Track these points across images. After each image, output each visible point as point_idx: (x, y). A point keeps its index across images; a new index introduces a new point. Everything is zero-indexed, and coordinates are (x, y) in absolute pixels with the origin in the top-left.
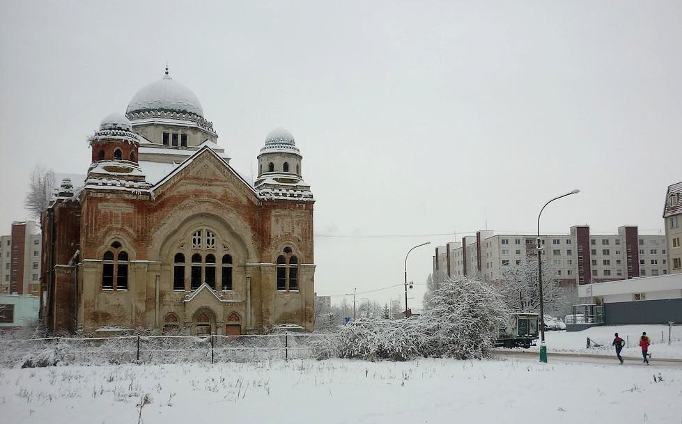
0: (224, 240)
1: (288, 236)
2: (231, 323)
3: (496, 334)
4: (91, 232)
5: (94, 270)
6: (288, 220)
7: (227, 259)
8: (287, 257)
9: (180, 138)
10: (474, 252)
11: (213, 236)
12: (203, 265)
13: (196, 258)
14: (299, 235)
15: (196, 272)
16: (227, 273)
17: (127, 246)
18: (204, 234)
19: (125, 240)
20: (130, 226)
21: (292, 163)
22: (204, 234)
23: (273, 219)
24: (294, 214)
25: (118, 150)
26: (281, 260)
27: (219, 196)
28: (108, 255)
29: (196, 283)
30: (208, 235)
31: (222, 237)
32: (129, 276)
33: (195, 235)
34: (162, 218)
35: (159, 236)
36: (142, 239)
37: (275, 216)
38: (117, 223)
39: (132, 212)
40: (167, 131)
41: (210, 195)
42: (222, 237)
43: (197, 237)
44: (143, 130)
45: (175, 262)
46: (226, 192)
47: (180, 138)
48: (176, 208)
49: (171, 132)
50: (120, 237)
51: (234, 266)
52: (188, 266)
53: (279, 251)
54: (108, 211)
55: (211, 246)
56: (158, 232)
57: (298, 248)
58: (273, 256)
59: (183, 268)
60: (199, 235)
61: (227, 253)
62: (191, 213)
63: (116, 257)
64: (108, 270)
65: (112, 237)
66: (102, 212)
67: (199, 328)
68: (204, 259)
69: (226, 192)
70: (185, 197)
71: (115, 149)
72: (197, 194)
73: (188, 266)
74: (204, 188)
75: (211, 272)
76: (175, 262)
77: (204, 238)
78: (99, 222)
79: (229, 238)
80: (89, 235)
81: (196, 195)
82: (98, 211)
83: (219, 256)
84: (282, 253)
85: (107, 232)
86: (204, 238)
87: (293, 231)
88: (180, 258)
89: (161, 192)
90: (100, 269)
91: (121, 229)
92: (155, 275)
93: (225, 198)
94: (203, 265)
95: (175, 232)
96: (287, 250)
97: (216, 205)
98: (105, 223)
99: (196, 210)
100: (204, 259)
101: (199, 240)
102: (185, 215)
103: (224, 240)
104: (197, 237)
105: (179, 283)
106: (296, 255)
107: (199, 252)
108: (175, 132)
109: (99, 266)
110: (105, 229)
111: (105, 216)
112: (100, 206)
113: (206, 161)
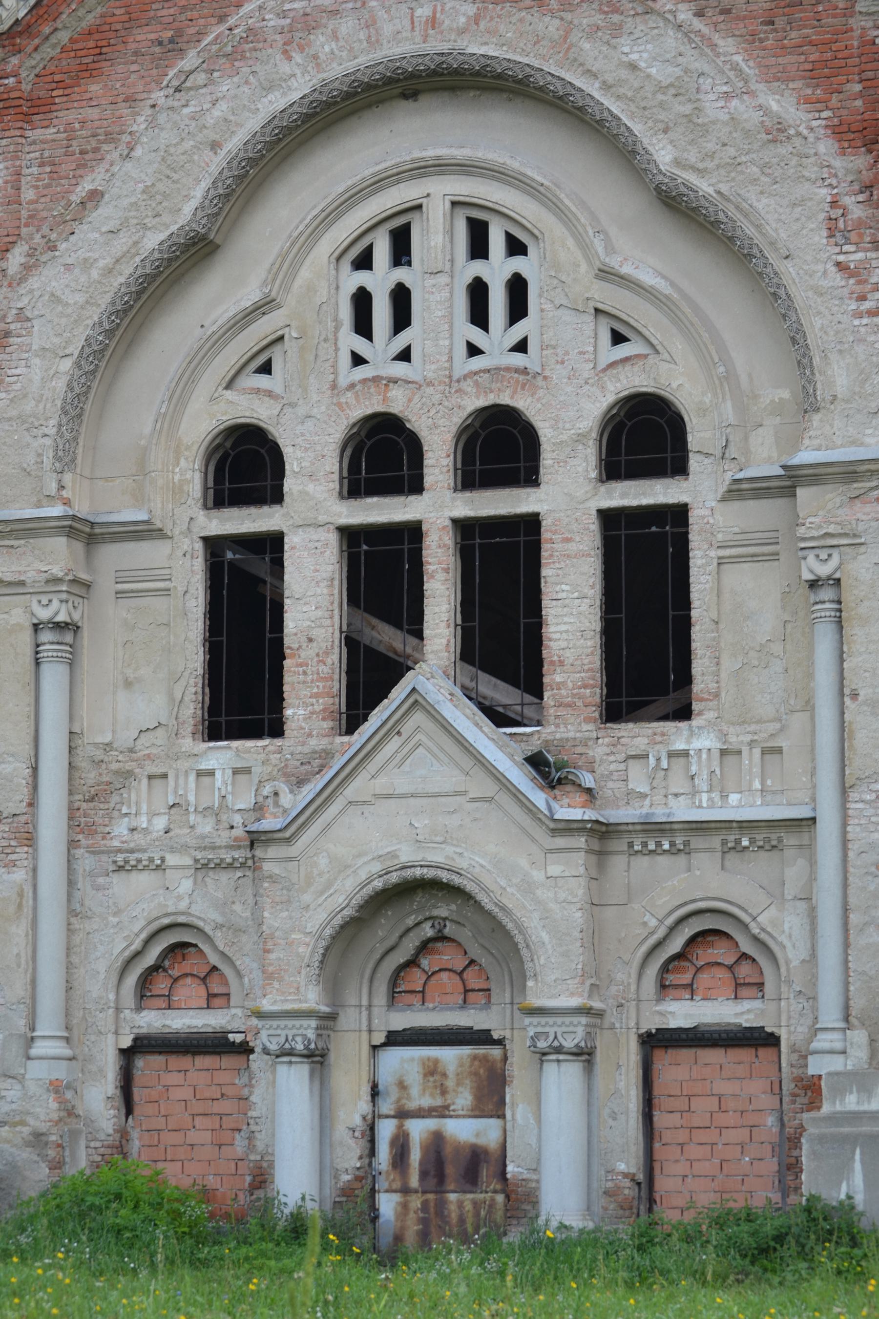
0: (606, 274)
2: (681, 1014)
7: (645, 435)
10: (415, 101)
11: (516, 247)
13: (382, 455)
15: (380, 570)
16: (647, 567)
18: (438, 238)
22: (438, 238)
30: (479, 248)
31: (585, 247)
33: (364, 262)
34: (88, 158)
42: (585, 237)
45: (679, 514)
48: (190, 60)
51: (697, 491)
52: (312, 520)
55: (383, 343)
56: (50, 279)
59: (271, 545)
60: (401, 252)
62: (295, 82)
68: (439, 461)
73: (312, 520)
75: (504, 561)
76: (679, 514)
77: (439, 273)
79: (653, 258)
83: (568, 421)
86: (439, 273)
88: (246, 465)
94: (438, 507)
95: (194, 252)
100: (439, 461)
101: (401, 298)
103: (606, 274)
104: (380, 280)
105: (242, 690)
107: (397, 403)
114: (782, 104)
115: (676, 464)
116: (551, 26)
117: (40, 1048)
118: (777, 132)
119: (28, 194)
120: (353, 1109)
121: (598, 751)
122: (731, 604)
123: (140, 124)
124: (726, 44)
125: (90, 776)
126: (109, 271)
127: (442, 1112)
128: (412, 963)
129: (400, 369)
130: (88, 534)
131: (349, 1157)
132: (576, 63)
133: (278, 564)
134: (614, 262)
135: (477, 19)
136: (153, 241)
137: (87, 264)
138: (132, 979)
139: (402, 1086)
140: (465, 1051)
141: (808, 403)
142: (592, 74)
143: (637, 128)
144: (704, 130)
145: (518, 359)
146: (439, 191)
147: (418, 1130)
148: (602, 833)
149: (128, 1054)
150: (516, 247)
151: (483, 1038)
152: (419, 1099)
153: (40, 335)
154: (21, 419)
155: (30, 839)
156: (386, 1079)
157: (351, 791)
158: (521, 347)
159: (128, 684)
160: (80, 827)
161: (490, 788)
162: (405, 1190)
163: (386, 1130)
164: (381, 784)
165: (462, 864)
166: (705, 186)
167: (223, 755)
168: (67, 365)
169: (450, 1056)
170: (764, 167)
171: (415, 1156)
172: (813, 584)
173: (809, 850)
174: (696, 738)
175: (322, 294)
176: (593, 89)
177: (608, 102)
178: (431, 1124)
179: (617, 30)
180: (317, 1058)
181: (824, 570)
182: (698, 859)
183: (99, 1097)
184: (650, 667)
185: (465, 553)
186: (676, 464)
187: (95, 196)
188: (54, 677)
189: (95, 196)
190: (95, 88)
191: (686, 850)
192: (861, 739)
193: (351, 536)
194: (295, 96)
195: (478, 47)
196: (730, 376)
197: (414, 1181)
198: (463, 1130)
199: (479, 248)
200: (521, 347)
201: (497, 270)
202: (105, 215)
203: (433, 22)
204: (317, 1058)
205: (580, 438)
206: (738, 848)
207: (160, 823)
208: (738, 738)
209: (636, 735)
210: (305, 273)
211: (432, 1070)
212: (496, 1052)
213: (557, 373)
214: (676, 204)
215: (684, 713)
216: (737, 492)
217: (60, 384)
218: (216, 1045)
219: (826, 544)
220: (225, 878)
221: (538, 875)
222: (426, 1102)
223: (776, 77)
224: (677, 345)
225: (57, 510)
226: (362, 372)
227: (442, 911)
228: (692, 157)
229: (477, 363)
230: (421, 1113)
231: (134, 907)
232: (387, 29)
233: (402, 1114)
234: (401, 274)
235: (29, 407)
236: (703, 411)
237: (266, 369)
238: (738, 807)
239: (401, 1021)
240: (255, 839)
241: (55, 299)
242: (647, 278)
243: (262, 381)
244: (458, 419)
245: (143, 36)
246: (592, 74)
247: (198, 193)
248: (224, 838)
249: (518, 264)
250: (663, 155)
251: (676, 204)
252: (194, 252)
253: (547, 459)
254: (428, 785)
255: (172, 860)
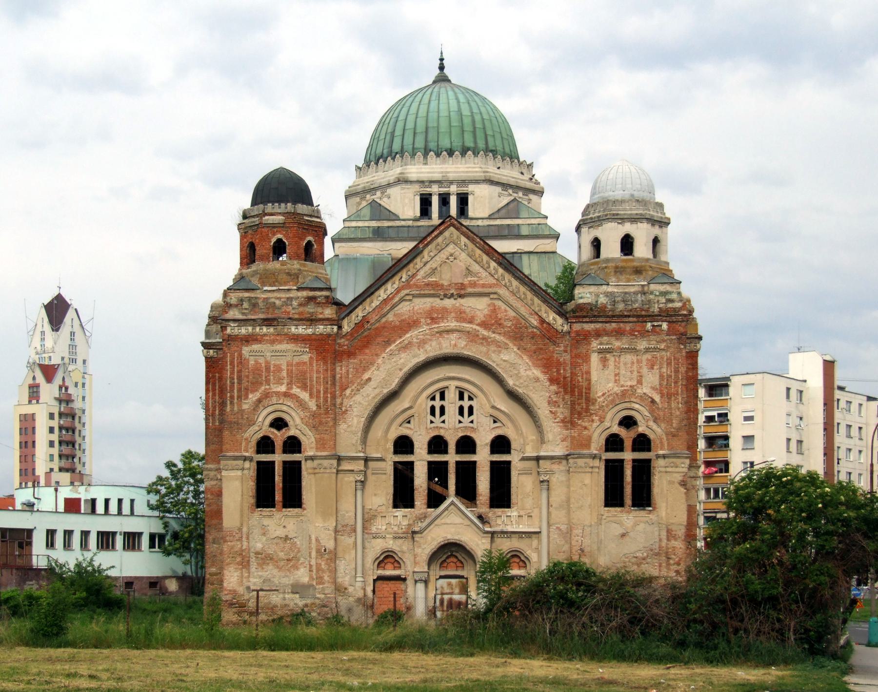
0: (493, 407)
1: (625, 395)
3: (85, 553)
4: (232, 403)
5: (239, 473)
6: (628, 358)
7: (501, 444)
8: (279, 437)
9: (435, 201)
11: (470, 398)
12: (452, 458)
13: (437, 444)
14: (653, 388)
15: (437, 471)
16: (501, 475)
17: (297, 427)
18: (452, 395)
19: (294, 414)
20: (304, 387)
21: (642, 234)
22: (452, 395)
23: (595, 358)
24: (642, 345)
25: (279, 241)
26: (613, 443)
27: (480, 317)
28: (265, 445)
29: (435, 500)
30: (461, 397)
32: (305, 483)
33: (433, 399)
34: (365, 369)
35: (359, 404)
36: (329, 413)
37: (600, 352)
38: (279, 382)
39: (306, 358)
40: (428, 190)
41: (461, 316)
42: (488, 398)
43: (437, 403)
44: (383, 193)
45: (509, 463)
46: (494, 310)
47: (435, 201)
48: (393, 347)
49: (435, 189)
50: (285, 408)
51: (514, 458)
52: (421, 459)
53: (607, 424)
54: (261, 360)
55: (437, 419)
56: (358, 398)
57: (652, 419)
58: (595, 436)
59: (411, 465)
60: (442, 398)
61: (404, 431)
63: (628, 444)
64: (264, 472)
65: (270, 409)
66: (252, 362)
67: (443, 582)
68: (452, 447)
69: (494, 310)
70: (410, 324)
71: (274, 240)
72: (434, 317)
73: (421, 459)
74: (448, 303)
75: (467, 472)
77: (452, 402)
78: (245, 384)
79: (504, 405)
80: (228, 409)
81: (432, 319)
82: (242, 362)
84: (616, 429)
85: (259, 401)
86: (452, 402)
87: (640, 382)
88: (404, 445)
89: (360, 318)
90: (250, 470)
91: (286, 395)
92: (354, 480)
93: (492, 322)
94: (452, 458)
95: (393, 396)
96: (628, 422)
97: (473, 337)
98: (256, 385)
99: (433, 350)
100: (452, 447)
102: (410, 360)
104: (437, 403)
105: (403, 495)
106: (648, 432)
107: (442, 433)
108: (443, 190)
109: (247, 464)
110: (258, 395)
111: (257, 370)
112: (246, 350)
113: (451, 248)
114: (537, 373)
115: (508, 451)
116: (484, 349)
117: (358, 579)
118: (537, 380)
119: (350, 376)
120: (432, 594)
121: (490, 515)
122: (522, 483)
123: (380, 361)
124: (525, 357)
125: (366, 516)
126: (374, 398)
127: (452, 593)
128: (445, 561)
129: (442, 425)
130: (366, 460)
131: (431, 604)
132: (490, 359)
133: (412, 469)
134: (496, 404)
135: (466, 345)
136: (385, 391)
137: (368, 395)
138: (376, 563)
139: (442, 587)
140: (457, 580)
141: (542, 441)
142: (494, 362)
143: (504, 376)
144: (520, 378)
145: (471, 425)
146: (453, 384)
147: (446, 597)
148: (493, 534)
149: (375, 581)
150: (470, 398)
151: (462, 577)
152: (447, 590)
153: (356, 411)
154: (351, 432)
155: (355, 531)
156: (438, 586)
157: (436, 522)
158: (472, 422)
159: (375, 495)
160: (364, 528)
161: (469, 523)
162: (443, 611)
163: (439, 597)
164: (443, 521)
165: (462, 539)
166: (520, 391)
167: (400, 512)
168: (363, 419)
169: (454, 581)
170: (534, 388)
171: (445, 603)
172: (542, 482)
173: (540, 541)
174: (513, 512)
175: (424, 406)
176: (494, 365)
177: (498, 369)
178: (449, 596)
179: (500, 352)
180: (426, 582)
181: (545, 479)
182: (513, 539)
183: (369, 589)
184: (501, 496)
185: (634, 468)
186: (508, 451)
187: (369, 379)
188: (359, 493)
189: (369, 379)
190: (367, 351)
191: (510, 537)
192: (553, 516)
193: (430, 463)
194: (421, 359)
195: (466, 353)
196: (522, 433)
197: (445, 608)
198: (457, 597)
199: (461, 397)
200: (472, 422)
201: (466, 404)
202: (372, 384)
203: (455, 345)
204: (426, 582)
205: (487, 444)
206: (522, 537)
207: (384, 527)
208: (522, 513)
209: (499, 511)
210: (419, 401)
211: (449, 584)
212: (464, 580)
213: (481, 429)
214: (513, 395)
215: (509, 506)
216: (524, 459)
217: (362, 425)
218: (398, 578)
219: (546, 473)
220: (401, 541)
221: (480, 542)
222: (448, 591)
223: (536, 366)
224: (509, 424)
225: (362, 455)
226: (433, 425)
227: (453, 549)
228: (517, 383)
229: (461, 425)
230: (447, 594)
231: (377, 547)
232: (444, 346)
233: (442, 594)
234: (442, 402)
235: (354, 429)
236: (515, 440)
237: (409, 422)
238: (521, 528)
239: (443, 573)
240: (414, 533)
241: (360, 403)
242: (503, 408)
243: (408, 425)
244: (457, 438)
245: (379, 340)
246: (494, 362)
247: (397, 380)
248: (400, 531)
249: (471, 403)
250: (511, 382)
251: (513, 395)
252: (393, 396)
253: (478, 449)
254: (454, 522)
255: (388, 536)
